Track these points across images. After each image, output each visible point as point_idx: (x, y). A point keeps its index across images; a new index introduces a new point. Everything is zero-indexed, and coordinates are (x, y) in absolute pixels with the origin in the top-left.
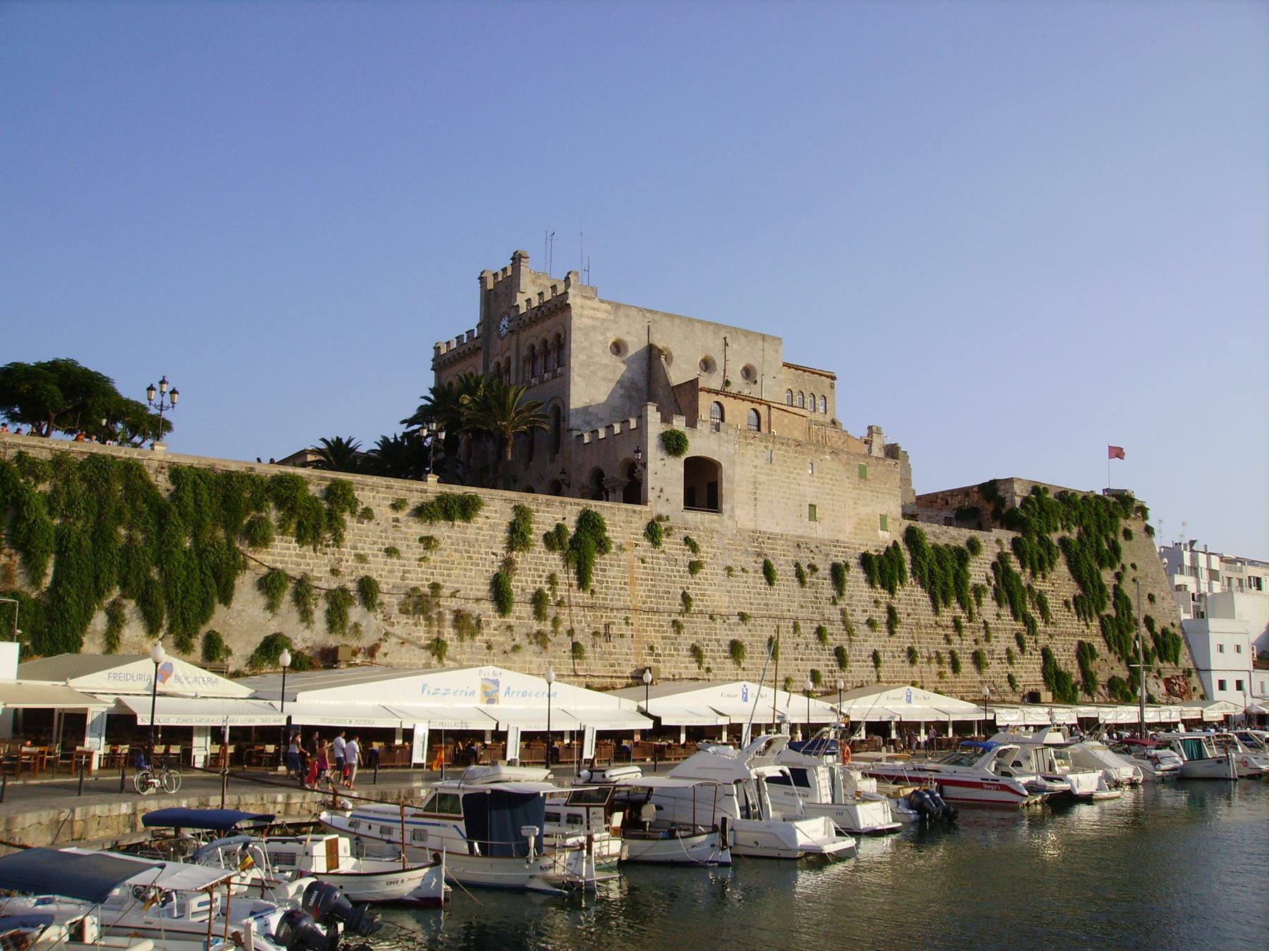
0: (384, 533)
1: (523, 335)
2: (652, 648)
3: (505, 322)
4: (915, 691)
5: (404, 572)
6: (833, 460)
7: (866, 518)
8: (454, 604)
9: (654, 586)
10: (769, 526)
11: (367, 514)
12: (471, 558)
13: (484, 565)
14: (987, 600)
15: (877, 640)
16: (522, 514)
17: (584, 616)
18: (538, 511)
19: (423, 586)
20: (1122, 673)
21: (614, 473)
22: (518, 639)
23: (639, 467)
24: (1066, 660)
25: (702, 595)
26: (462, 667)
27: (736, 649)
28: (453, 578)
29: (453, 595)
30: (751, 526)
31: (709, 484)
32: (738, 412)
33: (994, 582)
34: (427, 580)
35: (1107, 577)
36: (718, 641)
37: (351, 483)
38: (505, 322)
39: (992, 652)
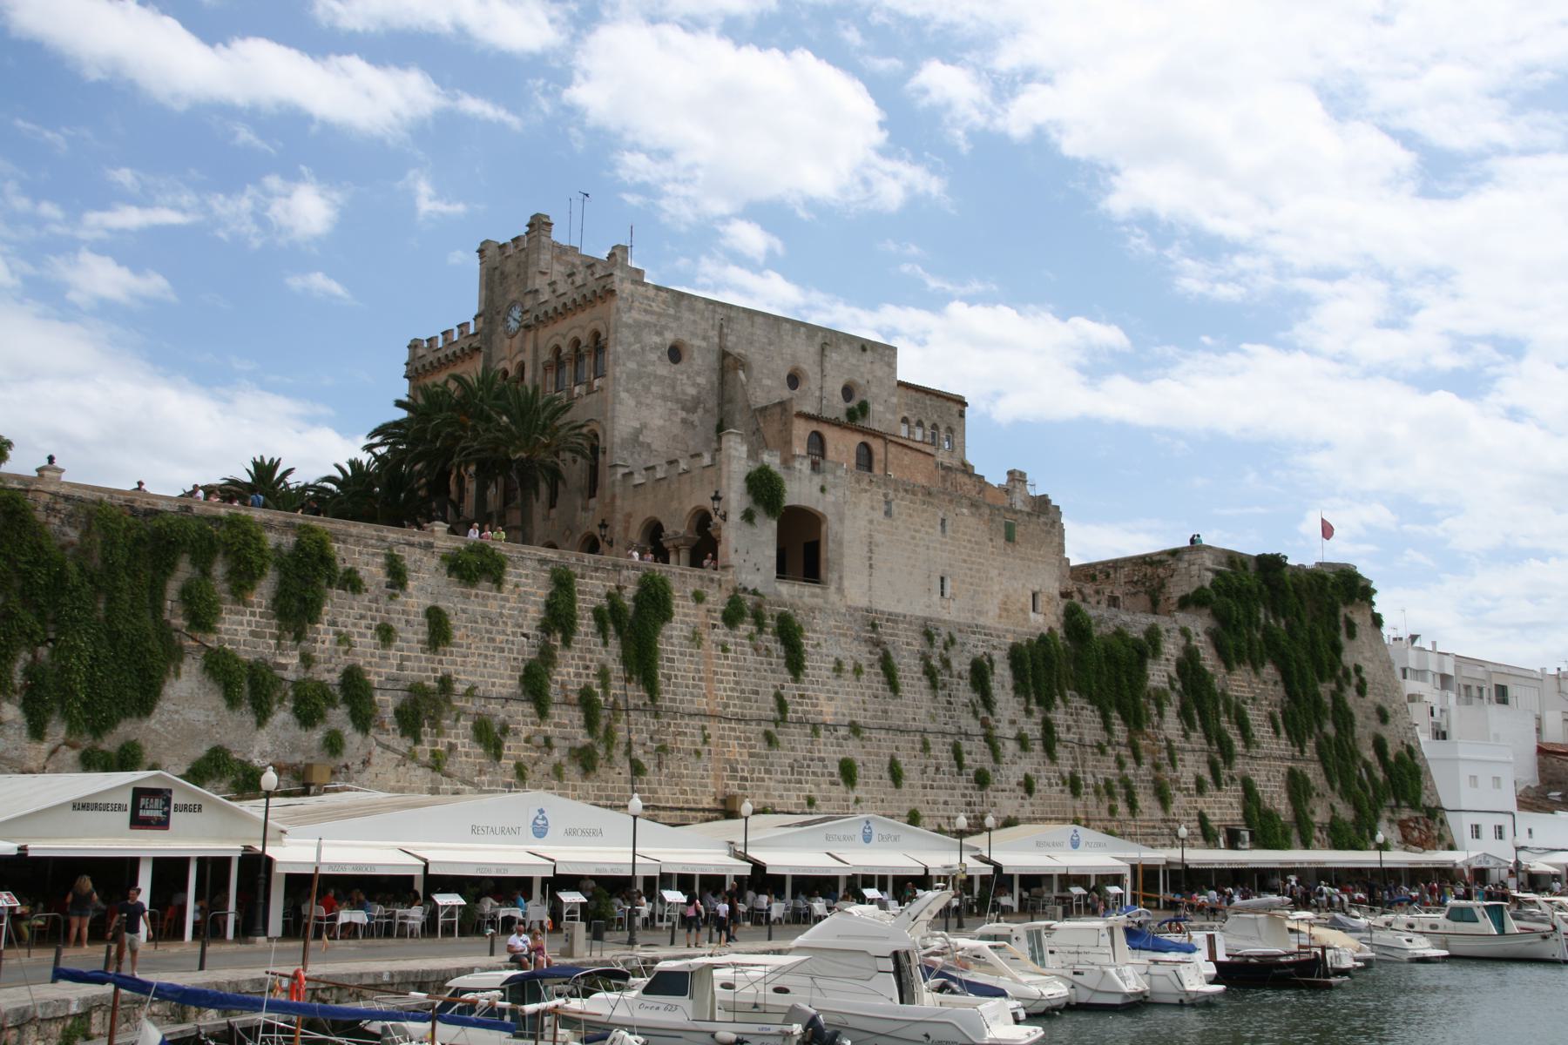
0: (392, 602)
1: (544, 334)
3: (516, 314)
4: (1081, 830)
5: (403, 658)
6: (973, 514)
7: (1006, 604)
8: (472, 706)
9: (737, 683)
12: (492, 640)
13: (511, 651)
14: (1171, 713)
15: (1031, 763)
16: (563, 583)
17: (646, 724)
18: (583, 577)
19: (428, 678)
20: (1346, 813)
21: (677, 526)
23: (716, 519)
24: (1276, 799)
25: (802, 696)
26: (482, 792)
27: (848, 772)
28: (469, 668)
31: (806, 545)
32: (843, 445)
33: (1178, 686)
34: (434, 670)
35: (1325, 689)
36: (822, 760)
38: (516, 314)
39: (1177, 781)
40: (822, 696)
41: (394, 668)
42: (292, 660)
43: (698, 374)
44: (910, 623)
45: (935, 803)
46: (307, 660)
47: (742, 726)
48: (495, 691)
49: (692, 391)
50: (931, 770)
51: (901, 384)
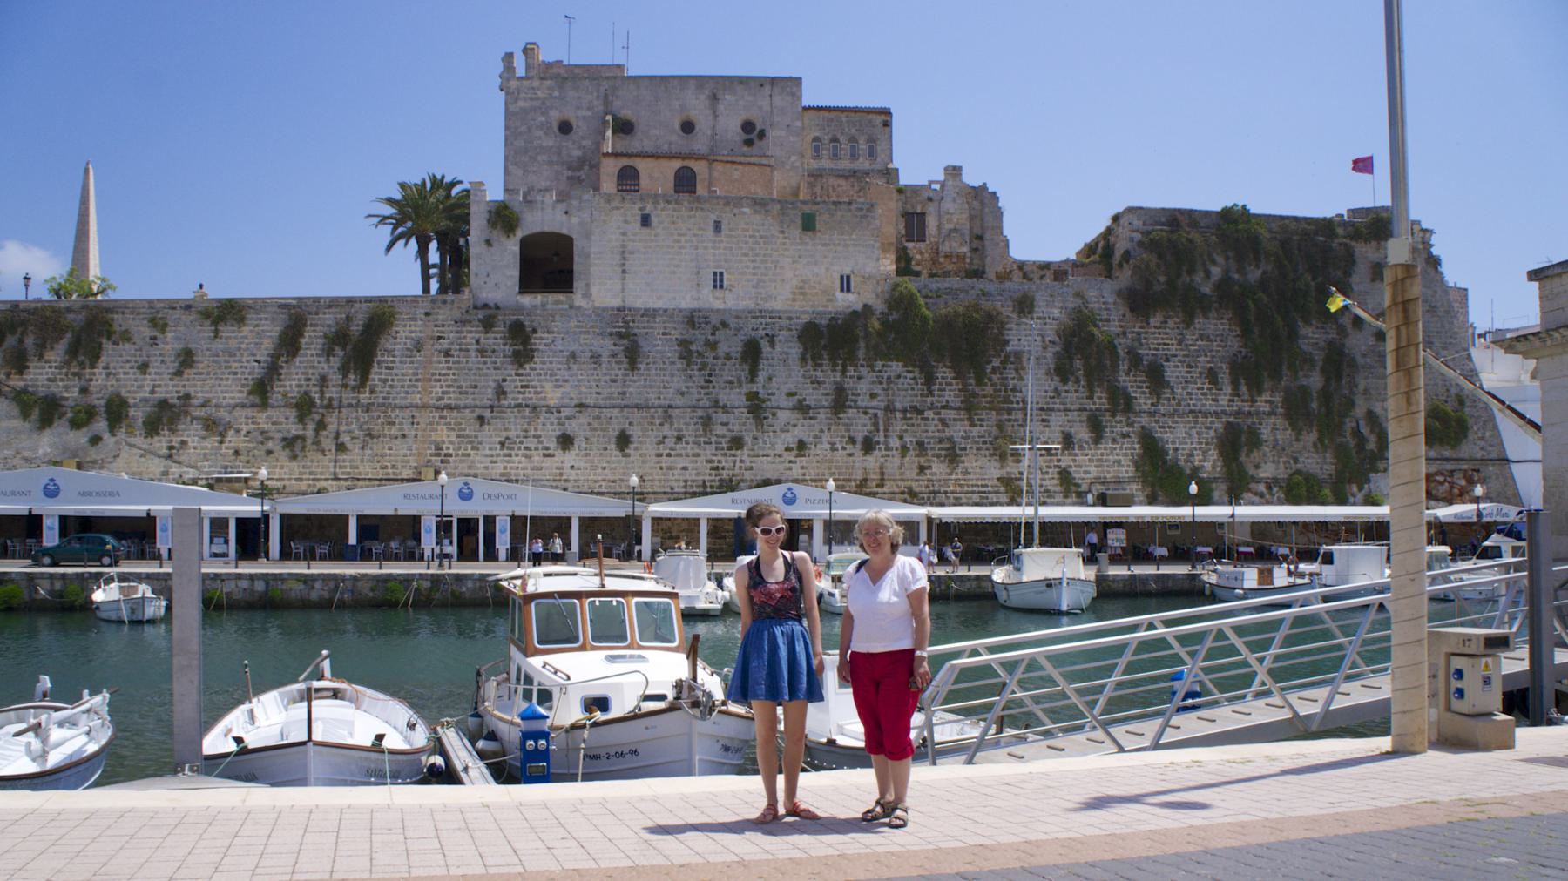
2: (439, 448)
10: (640, 299)
11: (126, 337)
17: (357, 418)
22: (779, 565)
29: (203, 405)
30: (617, 303)
37: (1152, 500)
40: (548, 386)
41: (140, 390)
42: (73, 394)
43: (583, 138)
44: (672, 316)
45: (670, 468)
46: (84, 391)
47: (454, 414)
48: (224, 402)
49: (577, 153)
50: (670, 442)
51: (805, 109)
